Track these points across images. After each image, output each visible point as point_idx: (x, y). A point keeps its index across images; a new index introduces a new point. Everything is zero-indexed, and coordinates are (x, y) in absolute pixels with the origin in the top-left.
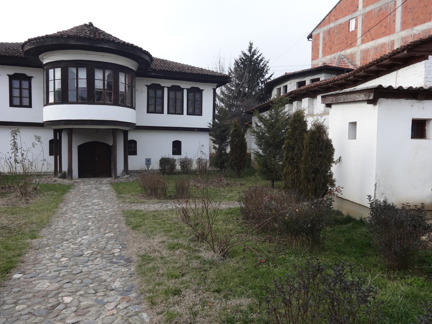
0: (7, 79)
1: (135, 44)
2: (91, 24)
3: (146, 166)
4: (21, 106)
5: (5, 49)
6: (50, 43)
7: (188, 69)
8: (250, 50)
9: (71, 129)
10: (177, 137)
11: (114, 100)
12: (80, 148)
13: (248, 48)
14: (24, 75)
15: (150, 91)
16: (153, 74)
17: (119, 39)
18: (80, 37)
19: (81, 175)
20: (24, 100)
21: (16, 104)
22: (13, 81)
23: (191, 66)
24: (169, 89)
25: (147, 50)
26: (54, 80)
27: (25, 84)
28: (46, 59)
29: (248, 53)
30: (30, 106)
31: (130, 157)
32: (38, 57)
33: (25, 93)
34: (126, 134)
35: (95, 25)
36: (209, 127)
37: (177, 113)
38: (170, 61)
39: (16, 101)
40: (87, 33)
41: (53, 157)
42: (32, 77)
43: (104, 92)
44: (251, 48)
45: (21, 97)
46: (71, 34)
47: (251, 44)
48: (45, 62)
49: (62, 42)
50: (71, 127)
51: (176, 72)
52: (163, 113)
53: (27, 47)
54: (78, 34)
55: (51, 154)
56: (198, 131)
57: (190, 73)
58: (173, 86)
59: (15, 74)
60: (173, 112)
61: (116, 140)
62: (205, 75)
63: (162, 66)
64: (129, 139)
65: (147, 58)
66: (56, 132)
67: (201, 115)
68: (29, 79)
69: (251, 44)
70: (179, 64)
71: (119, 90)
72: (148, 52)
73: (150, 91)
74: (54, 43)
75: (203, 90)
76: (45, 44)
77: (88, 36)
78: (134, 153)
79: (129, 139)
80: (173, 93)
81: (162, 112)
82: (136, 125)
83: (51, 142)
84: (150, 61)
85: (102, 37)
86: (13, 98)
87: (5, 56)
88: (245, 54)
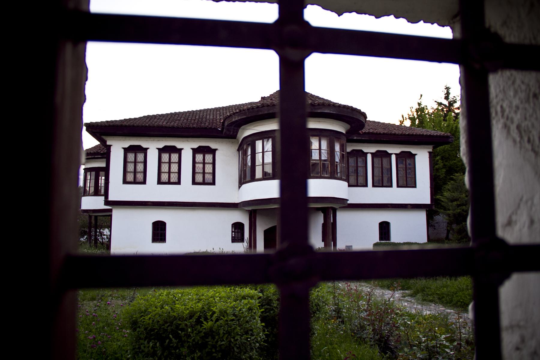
0: (122, 152)
6: (266, 112)
8: (447, 98)
11: (331, 173)
13: (444, 96)
14: (174, 147)
15: (375, 160)
16: (355, 138)
20: (162, 176)
21: (198, 181)
22: (137, 153)
24: (374, 155)
26: (263, 152)
27: (140, 157)
29: (446, 103)
30: (213, 183)
37: (172, 181)
39: (130, 177)
42: (216, 150)
43: (320, 164)
44: (448, 94)
45: (135, 172)
47: (448, 89)
53: (235, 118)
57: (401, 135)
58: (378, 151)
59: (200, 147)
67: (415, 187)
68: (213, 152)
69: (448, 89)
71: (335, 160)
75: (416, 154)
76: (260, 113)
80: (138, 155)
81: (366, 186)
82: (349, 202)
88: (440, 104)
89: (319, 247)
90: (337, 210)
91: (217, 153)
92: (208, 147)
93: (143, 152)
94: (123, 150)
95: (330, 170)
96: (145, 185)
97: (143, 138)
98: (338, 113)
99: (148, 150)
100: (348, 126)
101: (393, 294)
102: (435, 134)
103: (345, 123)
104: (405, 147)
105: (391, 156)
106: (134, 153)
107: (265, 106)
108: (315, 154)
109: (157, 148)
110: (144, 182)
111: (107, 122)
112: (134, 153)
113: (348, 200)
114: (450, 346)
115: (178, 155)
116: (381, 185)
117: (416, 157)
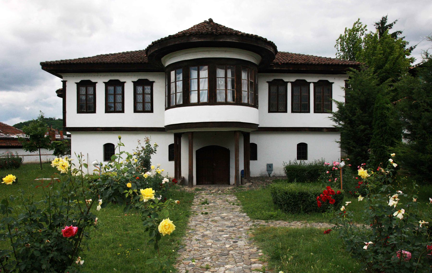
0: (75, 86)
1: (259, 35)
2: (211, 20)
3: (267, 172)
4: (144, 111)
5: (130, 57)
7: (314, 60)
9: (192, 133)
10: (112, 139)
12: (197, 152)
17: (240, 32)
18: (202, 34)
19: (198, 183)
21: (140, 110)
23: (317, 56)
25: (272, 41)
28: (169, 62)
30: (152, 111)
31: (252, 162)
32: (161, 59)
33: (148, 97)
34: (247, 136)
35: (215, 21)
36: (334, 126)
37: (116, 110)
38: (292, 54)
39: (140, 107)
40: (208, 29)
41: (173, 163)
42: (154, 82)
45: (144, 102)
46: (193, 32)
48: (167, 64)
49: (184, 41)
50: (193, 131)
51: (301, 64)
52: (287, 112)
54: (200, 31)
55: (170, 159)
56: (329, 131)
57: (318, 64)
60: (275, 110)
61: (238, 143)
62: (335, 65)
63: (284, 59)
64: (251, 142)
65: (272, 50)
66: (178, 137)
68: (151, 84)
70: (303, 55)
72: (273, 42)
73: (271, 88)
74: (177, 43)
77: (210, 31)
78: (255, 157)
79: (251, 141)
81: (286, 111)
82: (259, 126)
83: (171, 147)
84: (274, 53)
85: (223, 30)
86: (137, 103)
87: (131, 63)
89: (153, 190)
90: (250, 134)
91: (155, 85)
92: (147, 80)
93: (92, 86)
94: (76, 85)
95: (236, 97)
96: (95, 114)
97: (92, 74)
98: (241, 42)
99: (97, 84)
100: (259, 57)
101: (246, 245)
102: (350, 64)
103: (252, 52)
104: (323, 77)
105: (310, 85)
106: (85, 87)
107: (171, 38)
108: (221, 82)
109: (104, 82)
110: (123, 111)
111: (66, 60)
112: (85, 87)
113: (259, 125)
114: (404, 195)
115: (142, 88)
116: (299, 111)
117: (333, 85)
